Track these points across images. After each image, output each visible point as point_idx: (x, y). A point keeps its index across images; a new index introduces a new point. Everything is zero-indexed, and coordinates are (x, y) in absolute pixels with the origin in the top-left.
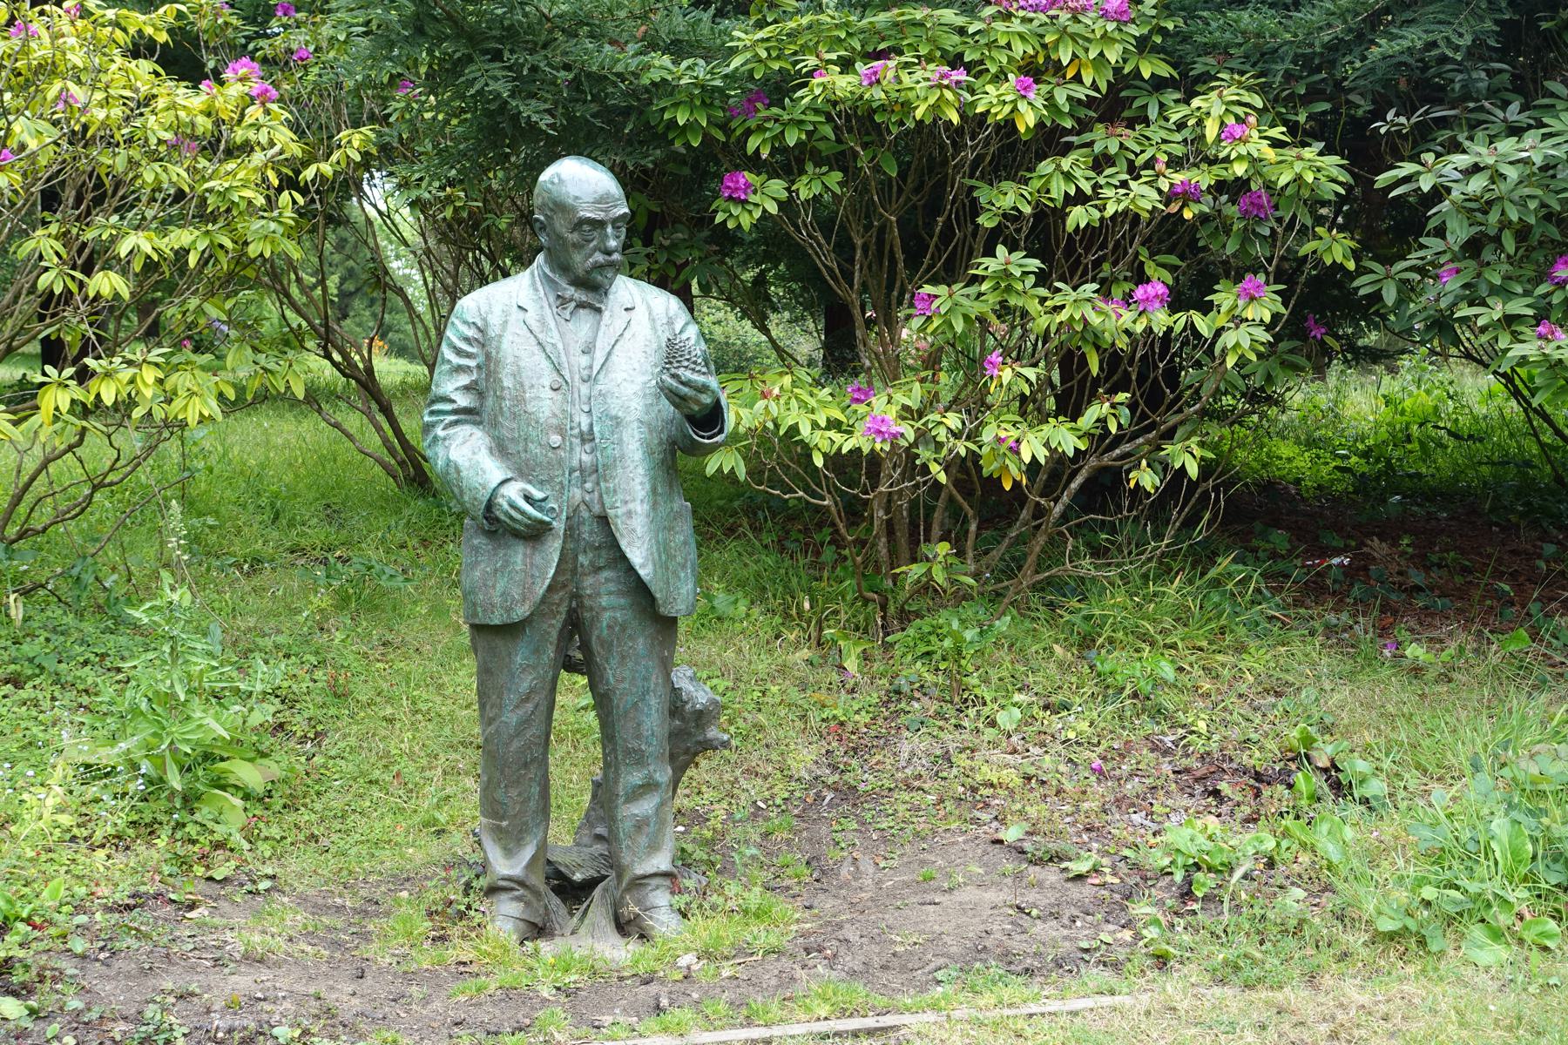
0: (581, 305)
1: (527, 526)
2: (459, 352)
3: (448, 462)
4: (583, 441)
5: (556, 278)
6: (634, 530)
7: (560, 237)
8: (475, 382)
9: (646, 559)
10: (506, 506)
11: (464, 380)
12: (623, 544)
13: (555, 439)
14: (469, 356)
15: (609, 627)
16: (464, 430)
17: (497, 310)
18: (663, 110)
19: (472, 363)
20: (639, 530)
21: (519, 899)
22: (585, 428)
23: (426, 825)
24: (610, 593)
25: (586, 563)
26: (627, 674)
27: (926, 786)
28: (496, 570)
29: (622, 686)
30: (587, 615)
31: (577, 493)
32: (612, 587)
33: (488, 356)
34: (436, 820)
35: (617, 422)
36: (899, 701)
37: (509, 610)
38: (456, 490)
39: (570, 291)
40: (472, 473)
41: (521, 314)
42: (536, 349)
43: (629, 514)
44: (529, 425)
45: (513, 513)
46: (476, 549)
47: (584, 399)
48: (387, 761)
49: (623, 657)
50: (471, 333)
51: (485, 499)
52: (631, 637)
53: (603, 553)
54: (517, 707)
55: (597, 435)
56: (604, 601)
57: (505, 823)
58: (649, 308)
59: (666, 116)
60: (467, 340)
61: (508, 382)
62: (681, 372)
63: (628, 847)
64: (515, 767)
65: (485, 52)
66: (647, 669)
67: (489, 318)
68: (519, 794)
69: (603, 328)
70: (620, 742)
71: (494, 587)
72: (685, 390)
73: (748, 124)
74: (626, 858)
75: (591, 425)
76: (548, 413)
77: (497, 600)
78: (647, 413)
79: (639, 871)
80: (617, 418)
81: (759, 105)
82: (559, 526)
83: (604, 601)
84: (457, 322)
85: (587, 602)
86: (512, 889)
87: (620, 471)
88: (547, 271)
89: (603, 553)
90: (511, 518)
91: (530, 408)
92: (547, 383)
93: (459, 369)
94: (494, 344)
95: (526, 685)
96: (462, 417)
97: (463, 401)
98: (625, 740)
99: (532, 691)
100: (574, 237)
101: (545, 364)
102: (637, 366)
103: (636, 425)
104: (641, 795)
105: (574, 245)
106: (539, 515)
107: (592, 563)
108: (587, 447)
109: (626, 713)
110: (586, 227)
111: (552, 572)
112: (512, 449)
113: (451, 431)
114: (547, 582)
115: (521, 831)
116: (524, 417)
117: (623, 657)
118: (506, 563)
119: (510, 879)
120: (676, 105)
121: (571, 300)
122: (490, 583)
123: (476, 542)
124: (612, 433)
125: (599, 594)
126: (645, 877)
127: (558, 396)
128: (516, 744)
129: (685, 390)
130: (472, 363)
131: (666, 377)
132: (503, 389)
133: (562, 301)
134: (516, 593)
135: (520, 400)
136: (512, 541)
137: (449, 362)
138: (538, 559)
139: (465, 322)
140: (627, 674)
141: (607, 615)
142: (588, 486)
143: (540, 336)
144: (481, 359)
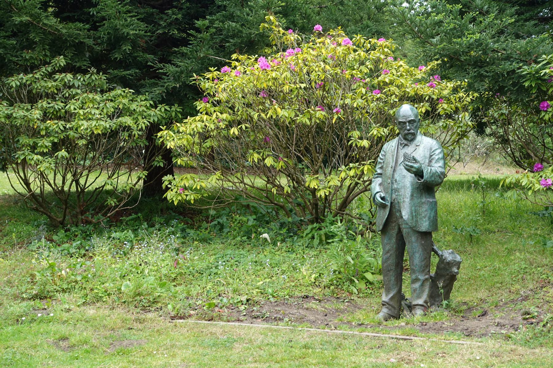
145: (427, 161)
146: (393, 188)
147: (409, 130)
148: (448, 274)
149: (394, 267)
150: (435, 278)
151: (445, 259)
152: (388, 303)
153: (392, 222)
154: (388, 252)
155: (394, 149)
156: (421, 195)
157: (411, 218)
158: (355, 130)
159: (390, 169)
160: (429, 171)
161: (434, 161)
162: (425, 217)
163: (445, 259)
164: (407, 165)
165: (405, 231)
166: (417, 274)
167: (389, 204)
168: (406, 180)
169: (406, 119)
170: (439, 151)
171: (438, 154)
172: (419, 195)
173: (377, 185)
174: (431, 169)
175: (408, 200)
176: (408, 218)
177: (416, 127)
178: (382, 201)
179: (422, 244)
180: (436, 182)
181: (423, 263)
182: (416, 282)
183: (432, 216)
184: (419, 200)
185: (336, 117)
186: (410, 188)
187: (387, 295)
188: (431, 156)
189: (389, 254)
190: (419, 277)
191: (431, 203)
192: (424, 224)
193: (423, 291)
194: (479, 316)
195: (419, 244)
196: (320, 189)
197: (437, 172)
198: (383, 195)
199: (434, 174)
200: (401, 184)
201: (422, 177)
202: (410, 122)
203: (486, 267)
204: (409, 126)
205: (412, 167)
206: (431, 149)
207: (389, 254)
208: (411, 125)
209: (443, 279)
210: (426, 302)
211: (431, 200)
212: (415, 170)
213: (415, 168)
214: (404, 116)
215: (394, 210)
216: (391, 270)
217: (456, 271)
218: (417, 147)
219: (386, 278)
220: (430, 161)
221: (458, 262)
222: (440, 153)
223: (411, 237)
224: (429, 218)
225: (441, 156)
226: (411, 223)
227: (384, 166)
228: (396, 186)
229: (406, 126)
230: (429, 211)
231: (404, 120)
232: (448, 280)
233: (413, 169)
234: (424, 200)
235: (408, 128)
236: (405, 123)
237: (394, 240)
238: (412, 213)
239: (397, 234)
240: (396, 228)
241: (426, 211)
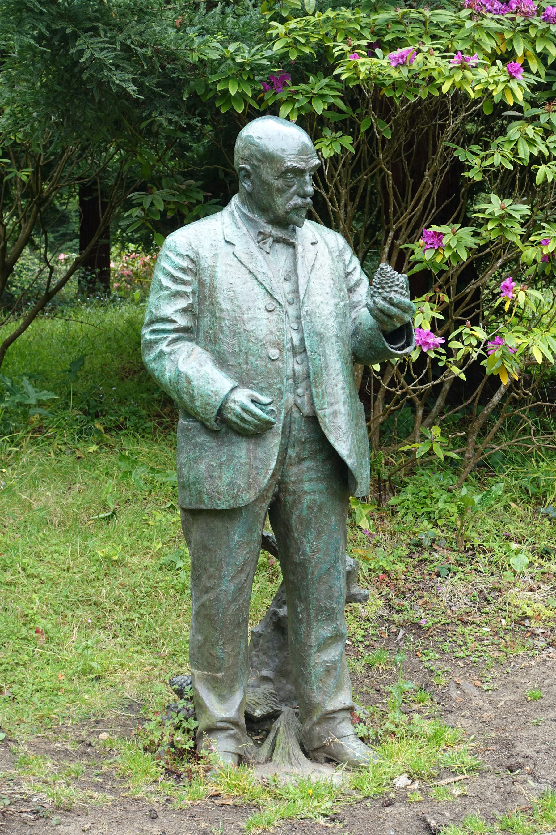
0: (277, 240)
1: (256, 426)
2: (176, 280)
3: (179, 374)
4: (295, 354)
5: (255, 217)
6: (340, 427)
7: (265, 183)
8: (191, 305)
9: (350, 450)
10: (238, 409)
11: (182, 303)
12: (331, 439)
13: (274, 353)
14: (185, 283)
15: (309, 507)
16: (184, 347)
17: (207, 244)
18: (215, 83)
19: (188, 289)
20: (344, 427)
21: (232, 737)
22: (296, 342)
23: (84, 672)
24: (311, 480)
25: (293, 455)
26: (322, 546)
27: (477, 621)
28: (221, 464)
29: (318, 556)
30: (290, 498)
31: (290, 398)
32: (312, 474)
33: (201, 284)
34: (92, 669)
35: (321, 337)
36: (422, 553)
37: (235, 497)
38: (185, 397)
39: (268, 229)
40: (202, 382)
41: (230, 248)
42: (248, 277)
43: (335, 414)
44: (249, 341)
45: (245, 416)
46: (201, 446)
47: (292, 318)
48: (27, 620)
49: (319, 532)
50: (185, 264)
51: (218, 405)
52: (326, 516)
53: (308, 446)
54: (234, 577)
55: (308, 348)
56: (306, 486)
57: (220, 675)
58: (326, 243)
59: (219, 88)
60: (183, 270)
61: (225, 305)
62: (392, 295)
63: (319, 688)
64: (231, 627)
65: (87, 30)
66: (337, 540)
67: (201, 251)
68: (233, 650)
69: (299, 256)
70: (313, 602)
71: (220, 478)
72: (394, 310)
73: (278, 96)
74: (317, 697)
75: (302, 340)
76: (265, 331)
77: (224, 489)
78: (341, 330)
79: (330, 708)
80: (320, 334)
81: (288, 82)
82: (279, 426)
83: (306, 486)
84: (170, 254)
85: (291, 487)
86: (228, 729)
87: (325, 378)
88: (246, 211)
89: (308, 446)
90: (243, 420)
91: (248, 327)
92: (262, 306)
93: (177, 294)
94: (208, 273)
95: (241, 558)
96: (181, 335)
97: (182, 321)
98: (318, 600)
99: (245, 563)
100: (279, 183)
101: (258, 289)
102: (328, 290)
103: (334, 340)
104: (329, 645)
105: (278, 190)
106: (267, 417)
107: (298, 456)
108: (299, 358)
109: (320, 578)
110: (290, 175)
111: (273, 464)
112: (232, 361)
113: (176, 347)
114: (270, 472)
115: (232, 680)
116: (244, 334)
117: (319, 532)
118: (231, 458)
119: (227, 721)
120: (227, 79)
121: (270, 236)
122: (216, 474)
123: (199, 440)
124: (318, 346)
125: (301, 481)
126: (334, 712)
127: (273, 317)
128: (233, 608)
129: (394, 310)
130: (188, 289)
131: (378, 300)
132: (222, 310)
133: (263, 236)
134: (242, 482)
135: (237, 321)
136: (235, 438)
137: (168, 288)
138: (260, 453)
139: (179, 255)
140: (322, 546)
141: (308, 498)
142: (300, 391)
143: (251, 267)
144: (195, 285)
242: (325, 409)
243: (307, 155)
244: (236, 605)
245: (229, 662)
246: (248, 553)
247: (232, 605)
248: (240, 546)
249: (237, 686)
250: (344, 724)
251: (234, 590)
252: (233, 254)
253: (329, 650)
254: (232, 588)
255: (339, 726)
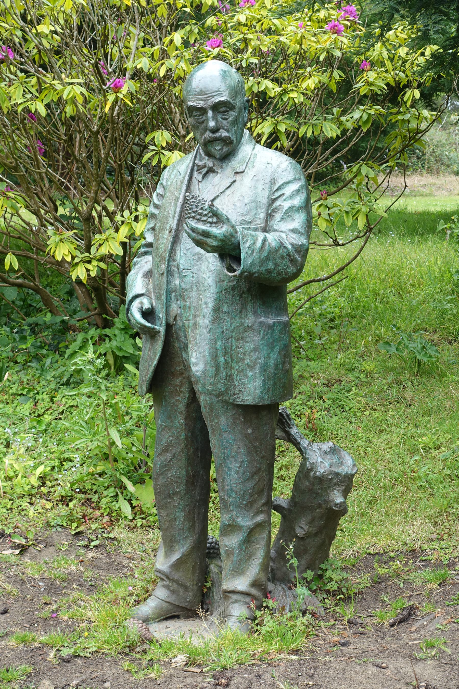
95: (165, 440)
145: (262, 215)
146: (173, 286)
147: (215, 131)
148: (320, 506)
149: (183, 487)
150: (289, 510)
151: (311, 470)
152: (168, 577)
153: (174, 375)
154: (166, 450)
155: (182, 182)
156: (243, 307)
157: (212, 370)
158: (158, 129)
159: (166, 234)
160: (259, 243)
161: (278, 216)
162: (252, 367)
163: (311, 470)
164: (193, 229)
165: (203, 399)
166: (234, 513)
167: (161, 328)
168: (204, 267)
169: (205, 100)
170: (295, 186)
171: (291, 197)
172: (238, 309)
173: (140, 275)
174: (265, 240)
175: (207, 321)
176: (204, 372)
177: (235, 122)
178: (143, 321)
179: (246, 436)
180: (279, 273)
181: (250, 485)
182: (232, 531)
183: (272, 363)
184: (238, 321)
185: (111, 98)
186: (213, 289)
187: (167, 555)
188: (274, 200)
189: (168, 456)
190: (240, 521)
191: (271, 327)
192: (251, 386)
193: (250, 556)
194: (392, 625)
195: (239, 436)
196: (77, 264)
197: (282, 245)
198: (147, 305)
199: (272, 253)
200: (188, 279)
201: (238, 259)
202: (216, 107)
203: (437, 447)
204: (214, 118)
205: (206, 234)
206: (273, 181)
207: (168, 456)
208: (219, 117)
209: (309, 517)
210: (255, 584)
211: (270, 321)
212: (215, 243)
213: (215, 237)
214: (201, 92)
215: (177, 345)
216: (176, 493)
217: (339, 500)
218: (238, 177)
219: (164, 514)
220: (269, 216)
221: (346, 476)
222: (298, 192)
223: (217, 417)
224: (264, 369)
225: (298, 201)
226: (214, 384)
227: (157, 227)
228: (177, 282)
229: (207, 120)
230: (264, 351)
231: (201, 104)
232: (321, 518)
233: (210, 241)
234: (250, 320)
235: (212, 124)
236: (203, 111)
237: (180, 420)
238: (215, 357)
239: (188, 405)
240: (185, 389)
241: (255, 350)
242: (190, 320)
243: (207, 94)
244: (164, 478)
245: (165, 524)
246: (170, 436)
247: (161, 477)
248: (163, 429)
249: (177, 547)
250: (236, 605)
251: (160, 465)
252: (235, 181)
253: (231, 537)
254: (159, 463)
255: (231, 606)
